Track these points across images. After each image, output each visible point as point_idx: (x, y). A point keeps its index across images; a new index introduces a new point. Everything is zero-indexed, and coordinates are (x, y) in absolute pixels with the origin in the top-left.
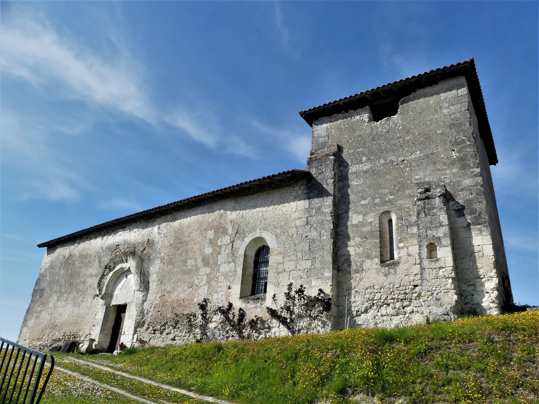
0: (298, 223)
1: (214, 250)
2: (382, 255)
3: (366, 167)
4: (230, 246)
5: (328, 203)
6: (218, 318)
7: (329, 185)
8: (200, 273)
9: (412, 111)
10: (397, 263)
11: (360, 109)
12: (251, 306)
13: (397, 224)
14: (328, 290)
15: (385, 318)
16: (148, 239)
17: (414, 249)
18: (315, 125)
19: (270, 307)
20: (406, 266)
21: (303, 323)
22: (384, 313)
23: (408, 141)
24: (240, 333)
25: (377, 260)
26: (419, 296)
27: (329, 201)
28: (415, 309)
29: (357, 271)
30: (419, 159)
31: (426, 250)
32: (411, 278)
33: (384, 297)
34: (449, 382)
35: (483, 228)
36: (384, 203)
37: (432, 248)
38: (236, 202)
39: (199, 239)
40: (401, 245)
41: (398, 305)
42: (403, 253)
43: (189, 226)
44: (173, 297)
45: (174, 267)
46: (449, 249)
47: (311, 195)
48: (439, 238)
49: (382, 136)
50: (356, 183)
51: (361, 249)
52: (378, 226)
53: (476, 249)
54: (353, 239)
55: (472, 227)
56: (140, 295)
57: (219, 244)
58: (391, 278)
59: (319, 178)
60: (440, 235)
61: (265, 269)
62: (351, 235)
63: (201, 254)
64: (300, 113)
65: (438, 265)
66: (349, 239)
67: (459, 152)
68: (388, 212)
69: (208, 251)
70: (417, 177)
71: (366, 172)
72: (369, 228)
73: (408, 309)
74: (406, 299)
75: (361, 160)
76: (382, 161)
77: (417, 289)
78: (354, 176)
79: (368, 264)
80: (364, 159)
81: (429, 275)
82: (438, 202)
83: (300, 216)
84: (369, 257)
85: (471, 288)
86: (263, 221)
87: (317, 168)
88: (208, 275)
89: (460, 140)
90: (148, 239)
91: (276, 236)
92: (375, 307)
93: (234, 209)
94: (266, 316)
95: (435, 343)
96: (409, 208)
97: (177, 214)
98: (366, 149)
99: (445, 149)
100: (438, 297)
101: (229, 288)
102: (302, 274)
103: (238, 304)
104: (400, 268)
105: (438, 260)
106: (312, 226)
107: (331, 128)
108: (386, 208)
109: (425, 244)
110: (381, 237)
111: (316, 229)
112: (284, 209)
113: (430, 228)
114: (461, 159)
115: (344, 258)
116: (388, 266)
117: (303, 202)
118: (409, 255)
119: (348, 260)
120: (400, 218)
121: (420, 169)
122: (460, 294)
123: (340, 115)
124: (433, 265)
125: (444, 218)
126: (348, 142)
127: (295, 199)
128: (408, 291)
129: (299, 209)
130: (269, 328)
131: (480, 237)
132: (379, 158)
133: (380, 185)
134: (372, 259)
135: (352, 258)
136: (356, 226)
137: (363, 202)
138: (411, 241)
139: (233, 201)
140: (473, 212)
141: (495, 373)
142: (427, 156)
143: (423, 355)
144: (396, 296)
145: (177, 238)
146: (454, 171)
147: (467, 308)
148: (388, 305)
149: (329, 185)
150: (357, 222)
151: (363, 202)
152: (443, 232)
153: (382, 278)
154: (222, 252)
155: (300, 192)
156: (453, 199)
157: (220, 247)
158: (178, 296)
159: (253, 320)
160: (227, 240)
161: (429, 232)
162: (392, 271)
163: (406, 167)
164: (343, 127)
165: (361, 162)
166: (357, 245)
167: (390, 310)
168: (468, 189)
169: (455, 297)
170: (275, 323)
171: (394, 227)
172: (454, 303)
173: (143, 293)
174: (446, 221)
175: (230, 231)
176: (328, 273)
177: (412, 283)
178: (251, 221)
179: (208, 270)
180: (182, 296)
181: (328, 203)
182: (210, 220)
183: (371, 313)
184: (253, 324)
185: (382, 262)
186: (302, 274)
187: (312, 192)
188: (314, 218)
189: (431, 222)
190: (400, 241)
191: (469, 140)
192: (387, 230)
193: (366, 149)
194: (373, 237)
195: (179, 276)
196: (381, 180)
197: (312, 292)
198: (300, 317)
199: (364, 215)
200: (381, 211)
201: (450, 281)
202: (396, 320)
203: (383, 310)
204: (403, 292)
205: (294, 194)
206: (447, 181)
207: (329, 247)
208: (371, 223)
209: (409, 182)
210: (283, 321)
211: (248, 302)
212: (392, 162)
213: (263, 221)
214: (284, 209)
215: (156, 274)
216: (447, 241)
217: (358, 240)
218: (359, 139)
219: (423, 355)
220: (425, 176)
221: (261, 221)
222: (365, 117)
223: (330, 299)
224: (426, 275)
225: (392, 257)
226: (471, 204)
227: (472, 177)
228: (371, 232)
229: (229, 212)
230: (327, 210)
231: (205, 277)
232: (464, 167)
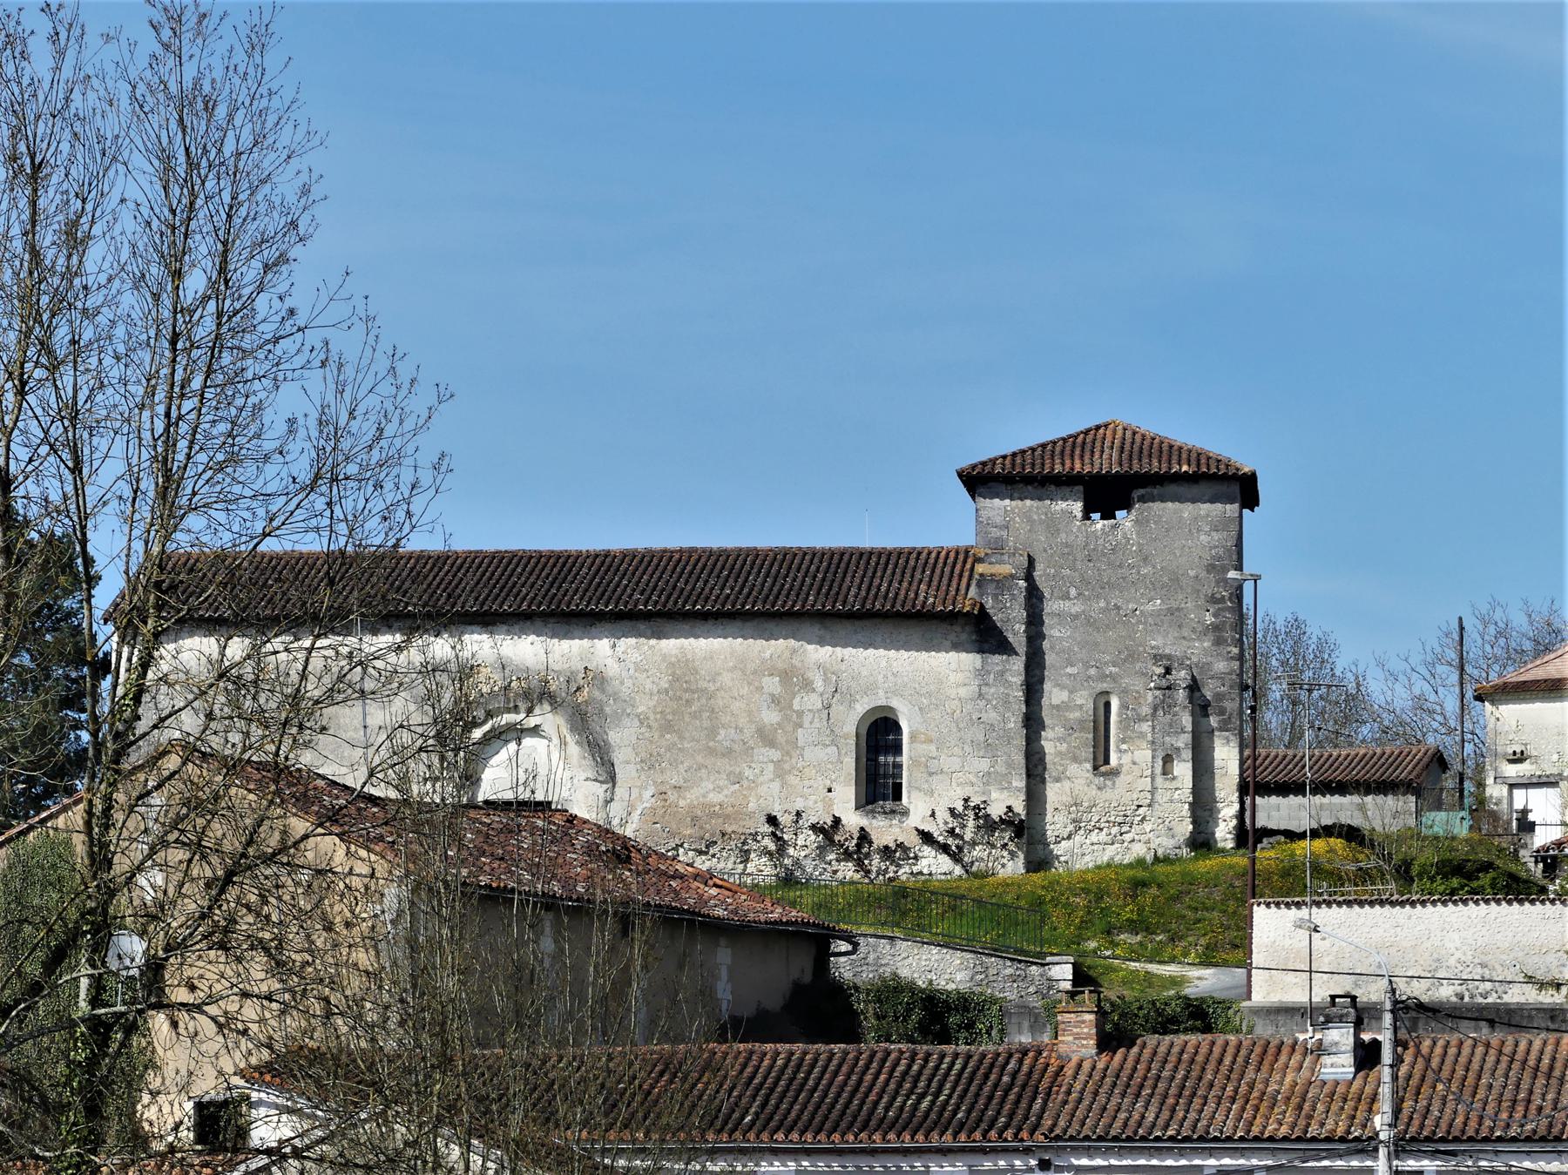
0: (963, 692)
1: (787, 718)
2: (1095, 759)
3: (1077, 608)
4: (825, 716)
5: (1016, 668)
6: (809, 839)
7: (1017, 633)
8: (756, 758)
9: (1155, 523)
10: (1115, 773)
11: (1069, 489)
12: (882, 823)
13: (1120, 714)
14: (1020, 808)
15: (1096, 847)
16: (586, 668)
17: (1144, 755)
18: (980, 496)
19: (921, 828)
20: (1129, 778)
21: (978, 852)
22: (1095, 841)
23: (1145, 576)
24: (860, 865)
25: (1089, 766)
26: (1143, 819)
27: (1017, 664)
28: (1137, 837)
29: (1058, 780)
30: (1158, 613)
31: (1161, 763)
32: (1135, 796)
33: (1095, 819)
34: (1199, 921)
35: (1232, 738)
36: (1103, 677)
37: (1168, 760)
38: (826, 628)
39: (745, 691)
40: (1124, 747)
41: (1115, 830)
42: (1126, 759)
43: (710, 657)
44: (691, 797)
45: (681, 738)
46: (1189, 765)
47: (986, 646)
48: (1178, 749)
49: (1104, 555)
50: (1058, 634)
51: (1065, 745)
52: (1091, 712)
53: (1217, 764)
54: (1053, 729)
55: (1216, 733)
56: (600, 790)
57: (796, 707)
58: (1108, 794)
59: (997, 618)
60: (1181, 745)
61: (890, 759)
62: (1047, 721)
63: (750, 721)
64: (960, 474)
65: (1174, 784)
66: (1043, 728)
67: (1215, 615)
68: (1108, 693)
69: (770, 717)
70: (1153, 643)
71: (1076, 617)
72: (1077, 714)
73: (1127, 837)
74: (1124, 823)
75: (1068, 592)
76: (1102, 604)
77: (1141, 811)
78: (1056, 620)
79: (1073, 769)
80: (1073, 592)
81: (1162, 797)
82: (1181, 695)
83: (967, 681)
84: (1075, 759)
85: (1207, 813)
86: (890, 678)
87: (995, 597)
88: (778, 764)
89: (1218, 596)
90: (586, 668)
91: (920, 709)
92: (1082, 832)
93: (822, 642)
94: (913, 840)
95: (1183, 888)
96: (1137, 692)
97: (669, 626)
98: (1077, 574)
99: (1197, 607)
100: (1171, 825)
101: (830, 790)
102: (974, 780)
103: (853, 820)
104: (1121, 781)
105: (1174, 778)
106: (989, 702)
107: (1012, 511)
108: (1105, 686)
109: (1160, 754)
110: (1095, 729)
111: (995, 707)
112: (934, 662)
113: (1168, 735)
114: (1216, 628)
115: (1037, 756)
116: (1104, 774)
117: (971, 656)
118: (1134, 763)
119: (1042, 760)
120: (1124, 707)
121: (1159, 631)
122: (1195, 822)
123: (1030, 488)
124: (1168, 784)
125: (1186, 721)
126: (1045, 551)
127: (957, 647)
128: (1129, 813)
129: (963, 668)
130: (916, 858)
131: (1226, 749)
132: (1098, 597)
133: (1096, 644)
134: (1080, 763)
135: (1048, 758)
136: (1057, 707)
137: (1069, 670)
138: (1138, 742)
139: (818, 626)
140: (1222, 712)
141: (1235, 912)
142: (1171, 612)
143: (1176, 898)
144: (1112, 819)
145: (676, 679)
146: (1205, 644)
147: (1201, 839)
148: (1101, 829)
149: (1017, 633)
150: (1059, 702)
151: (1069, 670)
152: (1183, 741)
153: (1094, 792)
154: (806, 724)
155: (964, 637)
156: (1199, 690)
157: (800, 714)
158: (704, 796)
159: (886, 847)
160: (812, 701)
161: (1167, 739)
162: (1109, 783)
163: (1139, 622)
164: (1035, 517)
165: (1066, 597)
166: (1059, 739)
167: (1103, 837)
168: (1220, 677)
169: (1191, 827)
170: (927, 851)
171: (1114, 718)
172: (1188, 834)
173: (605, 786)
174: (1189, 728)
175: (819, 684)
176: (1020, 782)
177: (1136, 803)
178: (865, 673)
179: (775, 754)
180: (714, 798)
181: (1016, 668)
182: (767, 655)
183: (1078, 838)
184: (887, 852)
185: (1096, 768)
186: (974, 780)
187: (986, 641)
188: (992, 690)
189: (1171, 726)
190: (1123, 741)
191: (1230, 599)
192: (1102, 718)
193: (1077, 574)
194: (1082, 729)
195: (699, 759)
196: (1099, 638)
197: (996, 811)
198: (974, 844)
199: (1071, 692)
200: (1098, 690)
201: (1187, 806)
202: (1110, 851)
203: (1094, 837)
204: (210, 575)
205: (952, 637)
206: (1195, 659)
207: (1021, 742)
208: (1081, 707)
209: (1141, 649)
210: (945, 848)
211: (874, 817)
212: (1117, 608)
213: (890, 678)
214: (934, 662)
215: (630, 749)
216: (1187, 754)
217: (1060, 731)
218: (1066, 550)
219: (1176, 898)
220: (1165, 644)
221: (885, 677)
222: (1077, 507)
223: (1022, 821)
224: (1158, 797)
225: (1107, 761)
226: (1221, 700)
227: (1227, 660)
228: (1081, 722)
229: (811, 648)
230: (1014, 680)
231: (771, 767)
232: (1219, 642)
